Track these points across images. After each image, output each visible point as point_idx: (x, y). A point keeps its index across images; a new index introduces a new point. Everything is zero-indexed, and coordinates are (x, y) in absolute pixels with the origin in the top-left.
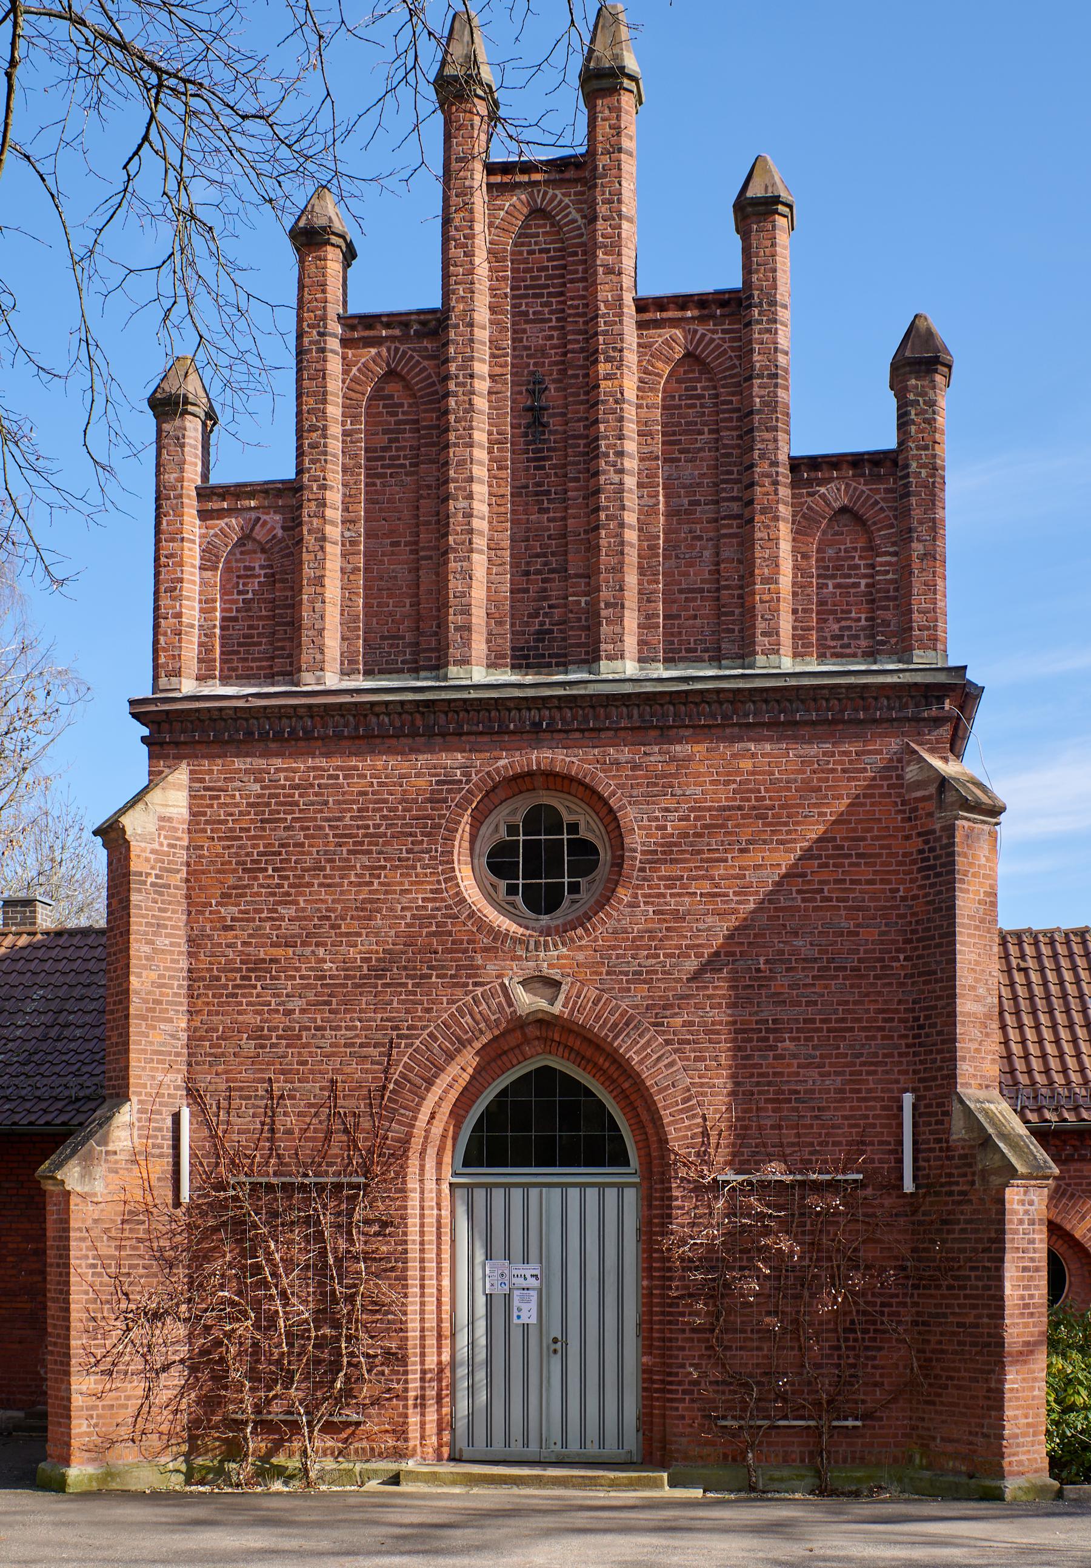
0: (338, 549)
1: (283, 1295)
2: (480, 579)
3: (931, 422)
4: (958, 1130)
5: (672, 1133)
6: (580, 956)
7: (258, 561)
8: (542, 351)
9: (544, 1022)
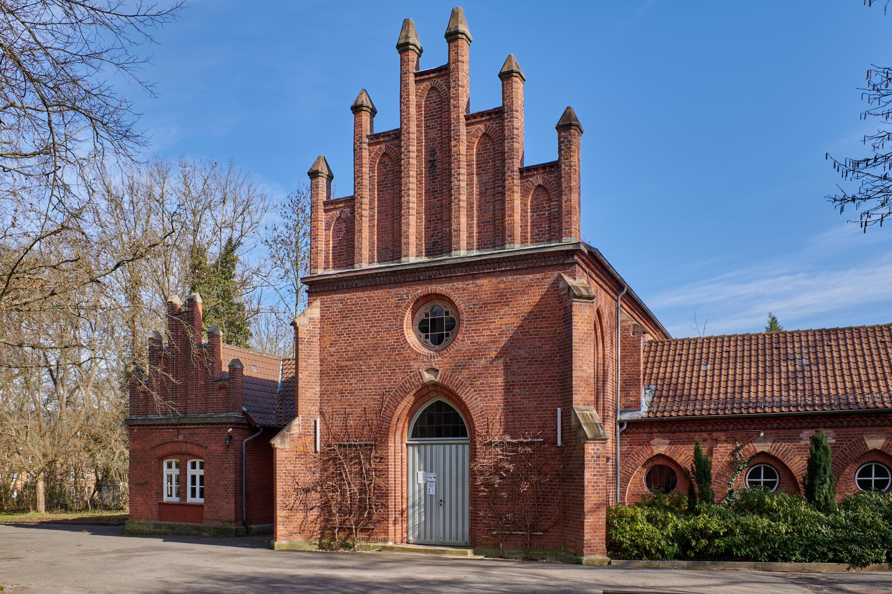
0: (367, 219)
1: (349, 483)
2: (414, 225)
3: (569, 148)
4: (573, 423)
5: (476, 424)
6: (445, 360)
7: (343, 226)
8: (435, 139)
9: (435, 384)
